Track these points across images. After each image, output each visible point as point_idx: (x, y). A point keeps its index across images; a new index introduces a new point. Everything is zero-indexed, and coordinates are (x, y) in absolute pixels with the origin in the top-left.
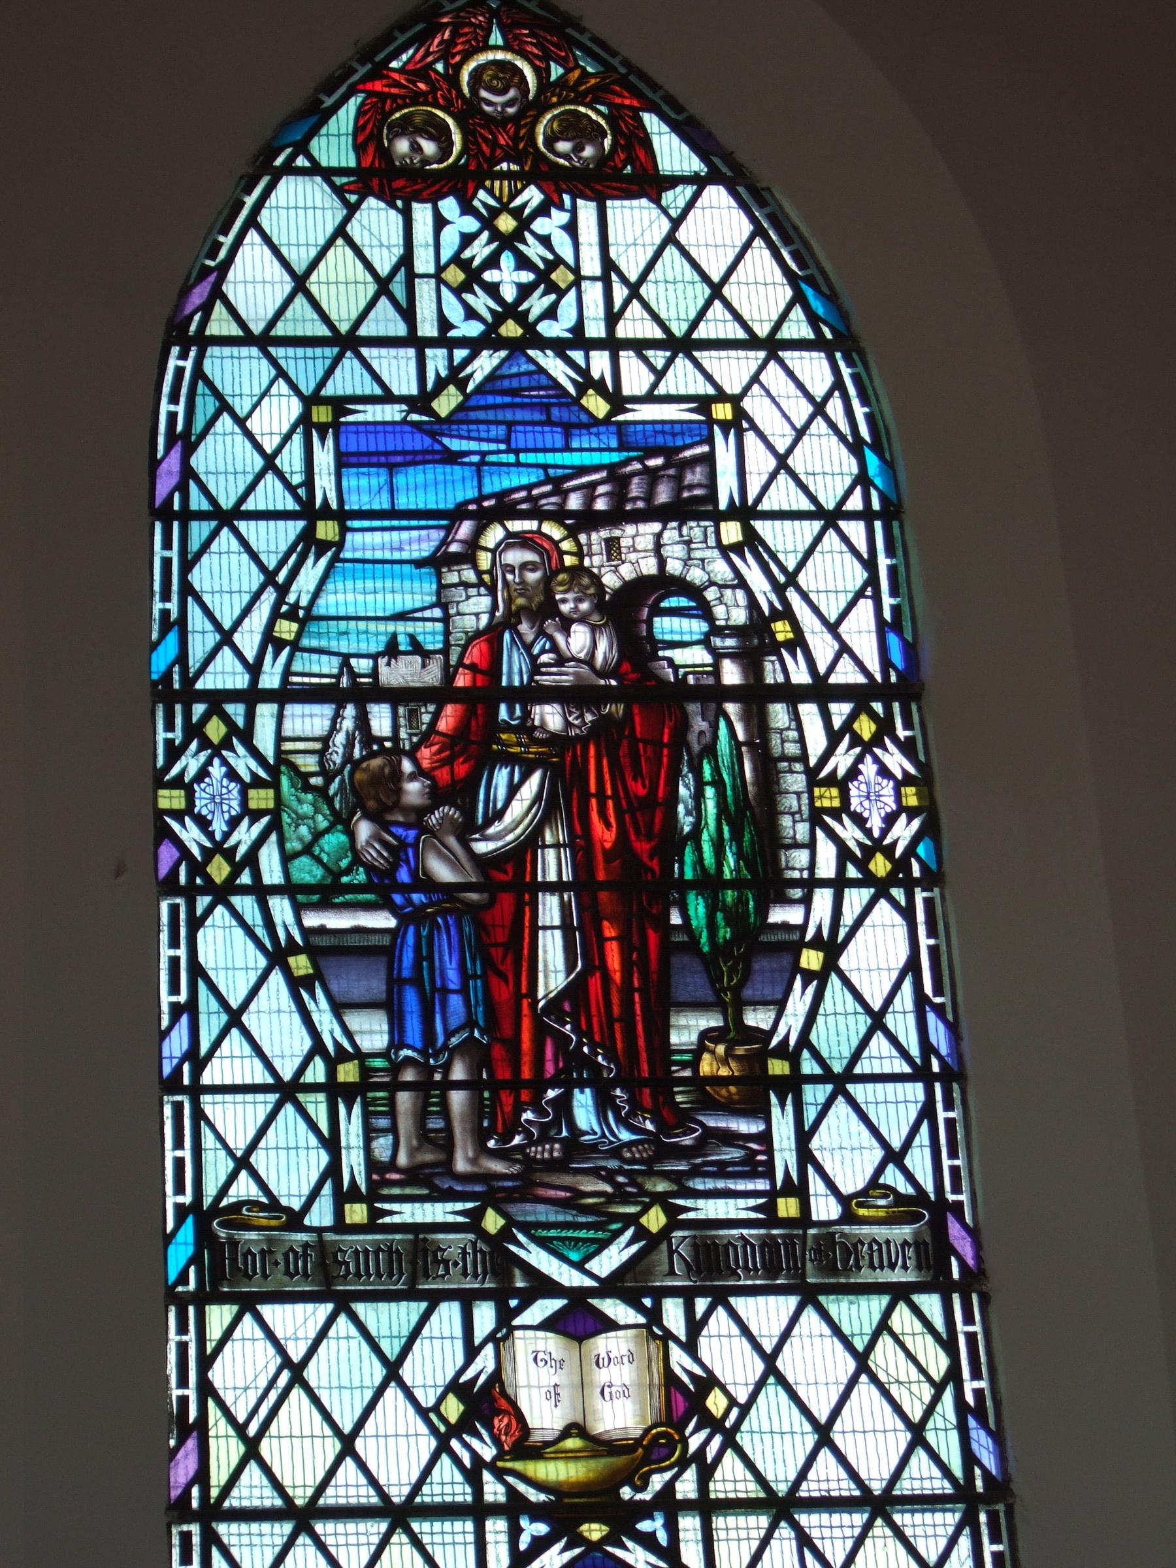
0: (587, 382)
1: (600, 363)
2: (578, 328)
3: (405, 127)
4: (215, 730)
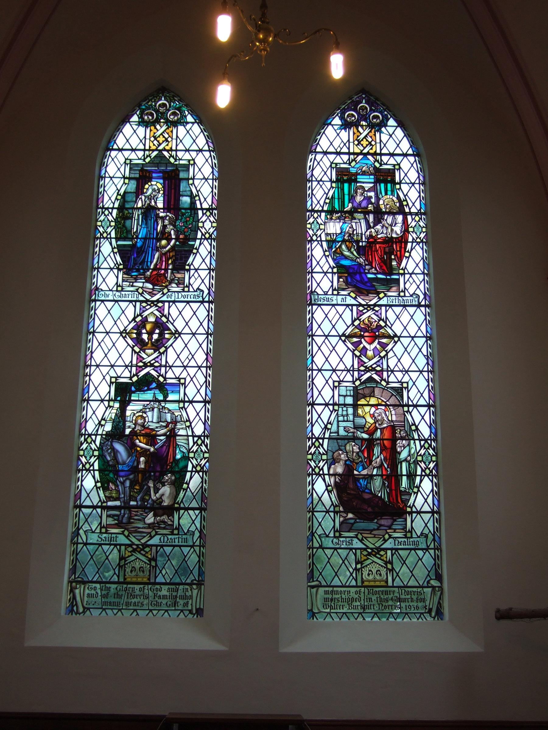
0: (171, 156)
1: (174, 153)
2: (171, 148)
3: (147, 114)
4: (89, 440)
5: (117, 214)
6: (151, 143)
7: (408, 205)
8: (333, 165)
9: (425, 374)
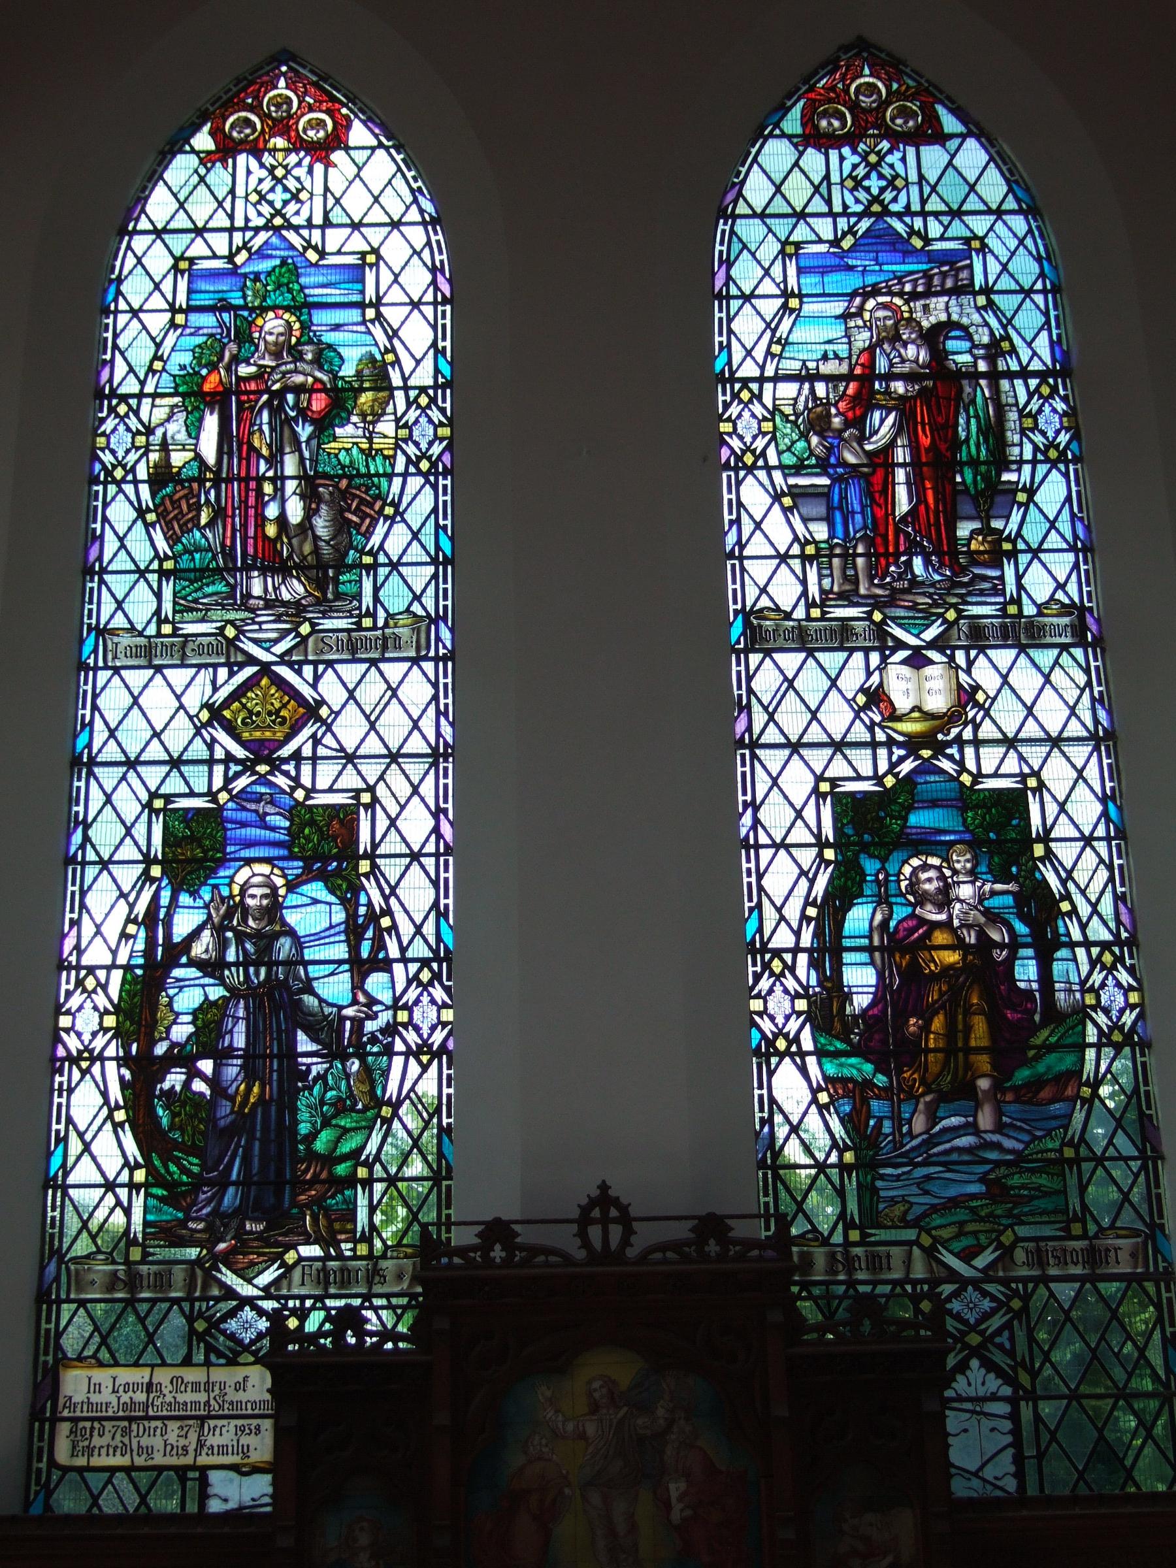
4: (90, 983)
5: (121, 991)
6: (250, 208)
7: (1074, 911)
8: (825, 787)
9: (1039, 299)
